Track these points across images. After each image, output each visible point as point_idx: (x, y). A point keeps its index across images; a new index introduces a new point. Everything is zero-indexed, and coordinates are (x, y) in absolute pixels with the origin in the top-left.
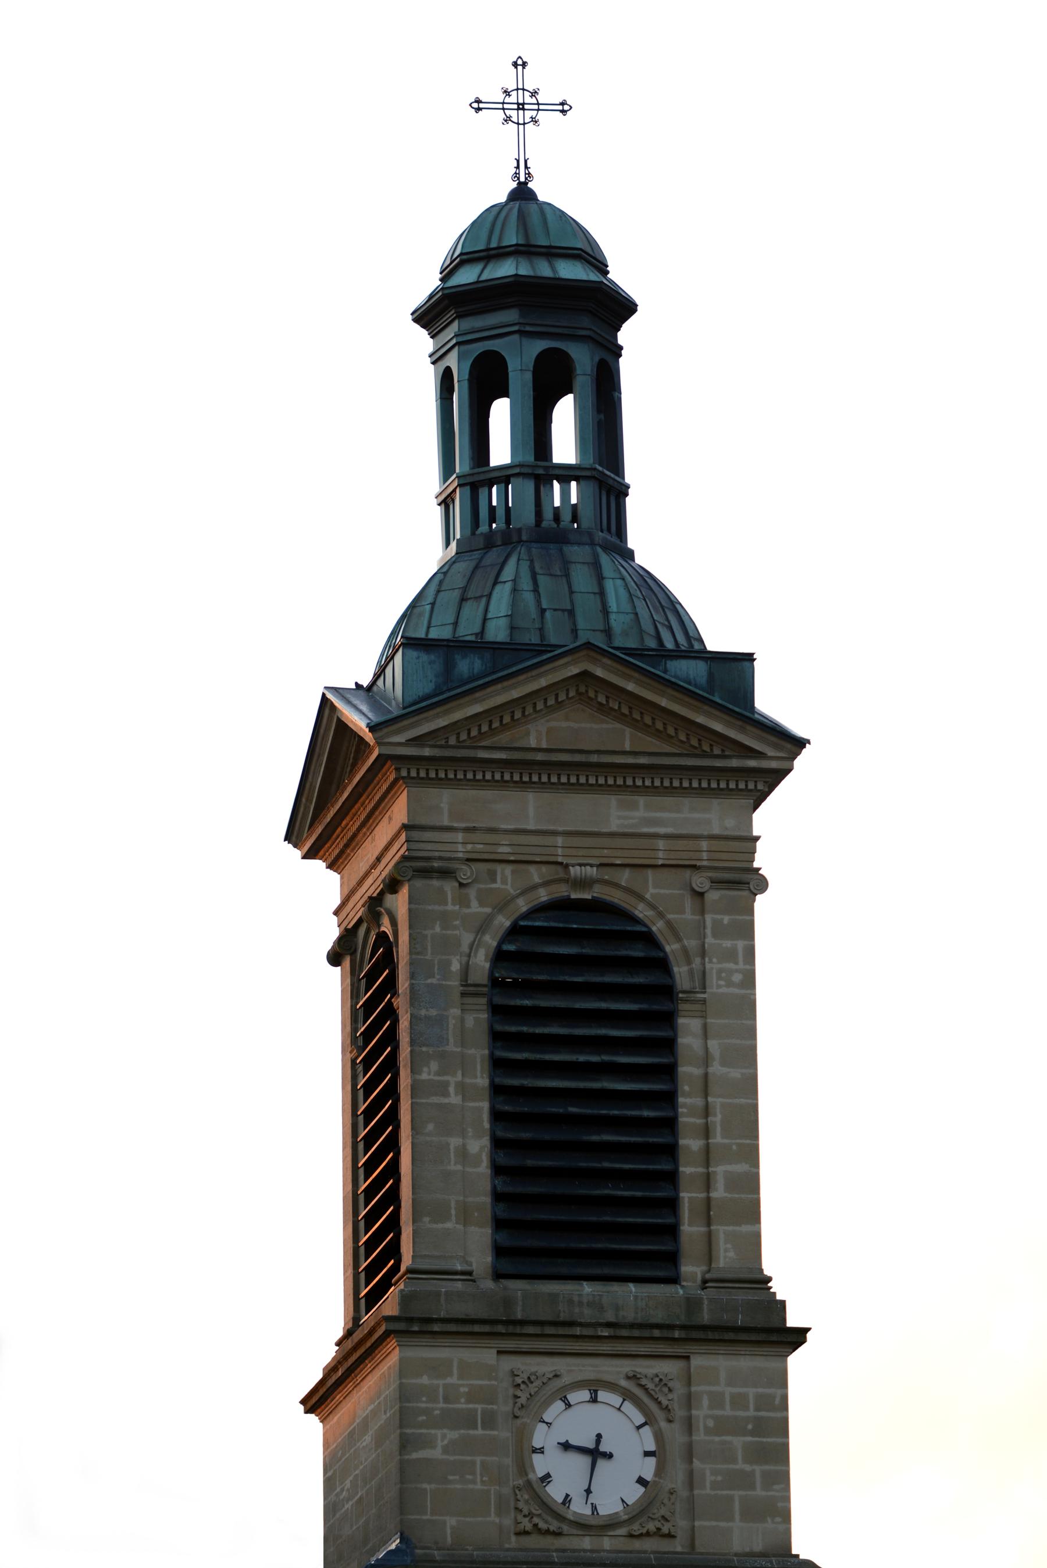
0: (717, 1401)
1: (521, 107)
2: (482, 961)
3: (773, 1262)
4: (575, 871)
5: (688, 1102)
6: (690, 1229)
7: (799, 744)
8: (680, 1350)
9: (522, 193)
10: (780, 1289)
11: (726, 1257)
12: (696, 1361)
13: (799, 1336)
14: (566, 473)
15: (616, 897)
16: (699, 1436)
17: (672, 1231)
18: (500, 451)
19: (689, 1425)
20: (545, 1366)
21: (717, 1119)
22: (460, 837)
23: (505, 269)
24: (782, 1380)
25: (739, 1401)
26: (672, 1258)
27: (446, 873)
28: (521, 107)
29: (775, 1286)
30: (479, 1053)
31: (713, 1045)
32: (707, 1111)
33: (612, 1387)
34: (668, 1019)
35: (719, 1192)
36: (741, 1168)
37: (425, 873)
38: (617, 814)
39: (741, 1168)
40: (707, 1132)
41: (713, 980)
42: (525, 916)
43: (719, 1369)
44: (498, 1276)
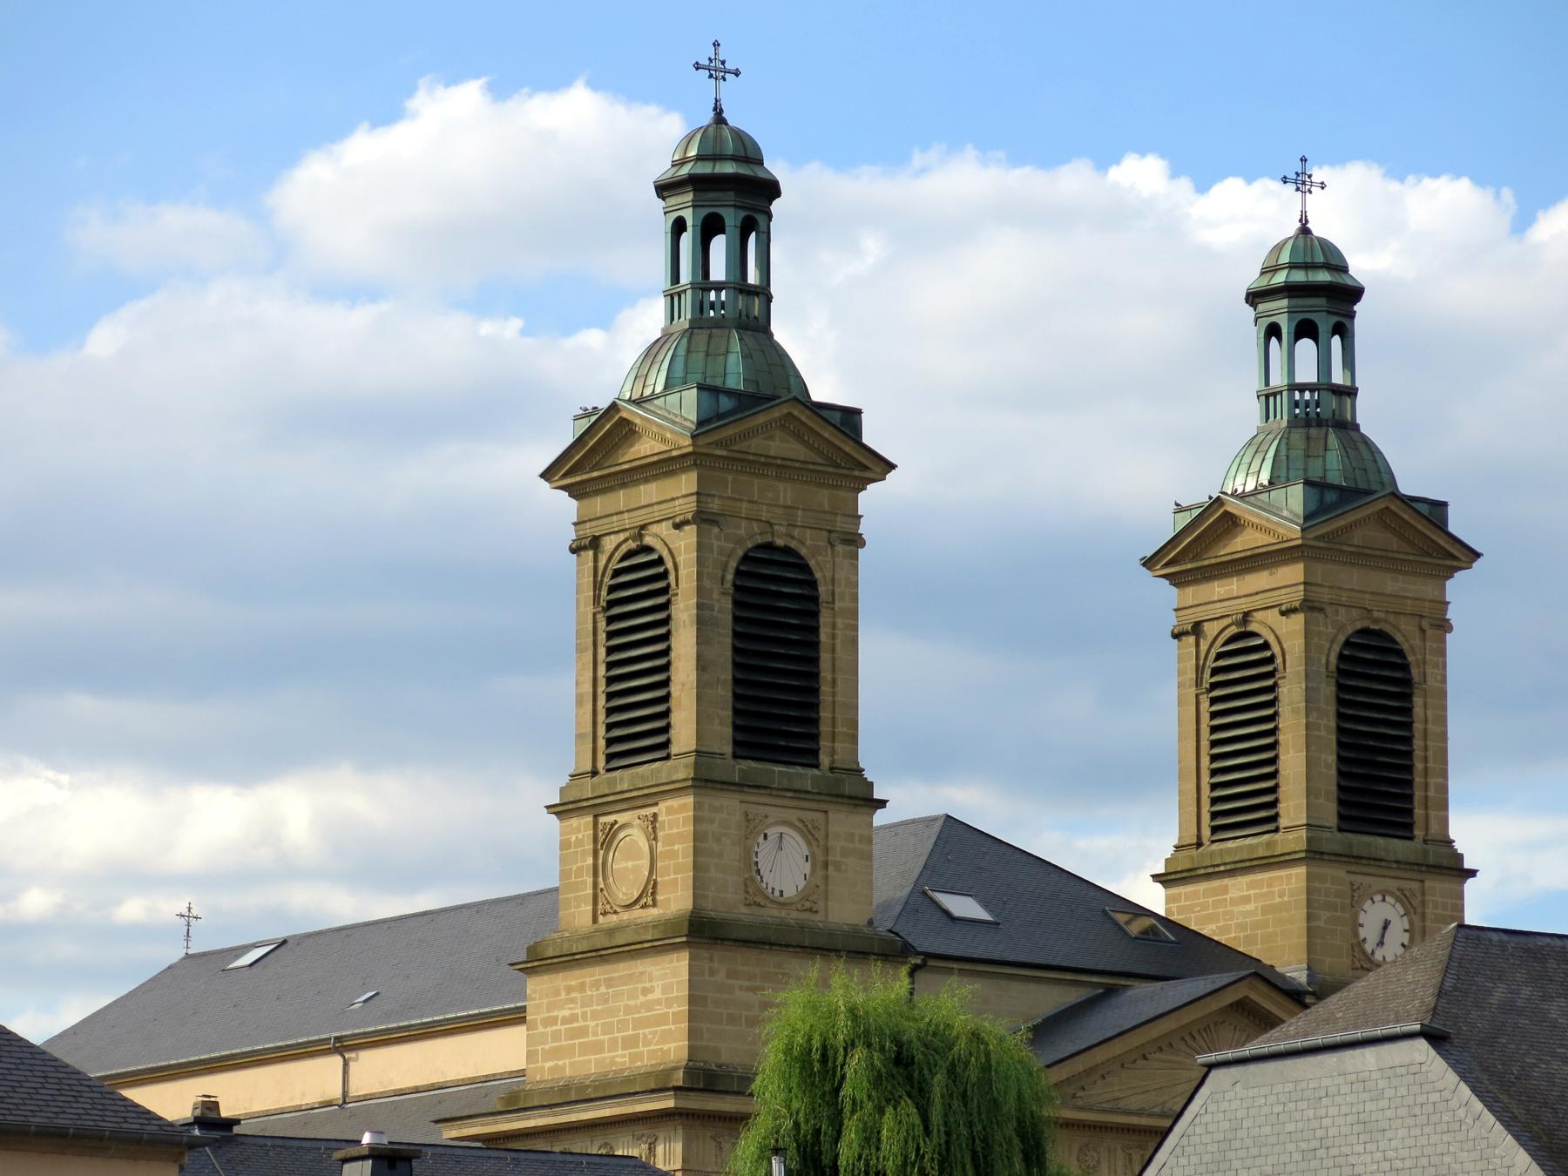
0: (1436, 907)
1: (717, 70)
2: (1333, 659)
3: (1453, 833)
4: (1376, 614)
5: (1417, 743)
6: (1418, 812)
7: (1478, 555)
8: (823, 806)
9: (1305, 230)
10: (1459, 846)
11: (841, 759)
12: (1428, 884)
13: (1472, 873)
14: (719, 287)
15: (1388, 629)
16: (1428, 923)
17: (1410, 812)
18: (718, 272)
19: (1423, 917)
20: (1367, 880)
21: (1430, 753)
22: (1326, 590)
23: (729, 168)
24: (1461, 896)
25: (1444, 906)
26: (1409, 827)
27: (1321, 610)
28: (717, 70)
29: (1457, 845)
30: (1332, 708)
31: (1429, 713)
32: (1426, 748)
33: (1392, 894)
34: (1408, 697)
35: (1431, 793)
36: (1441, 780)
37: (1312, 609)
38: (1392, 584)
39: (1441, 780)
40: (1426, 760)
41: (1430, 680)
42: (750, 550)
43: (1437, 886)
44: (1340, 830)
